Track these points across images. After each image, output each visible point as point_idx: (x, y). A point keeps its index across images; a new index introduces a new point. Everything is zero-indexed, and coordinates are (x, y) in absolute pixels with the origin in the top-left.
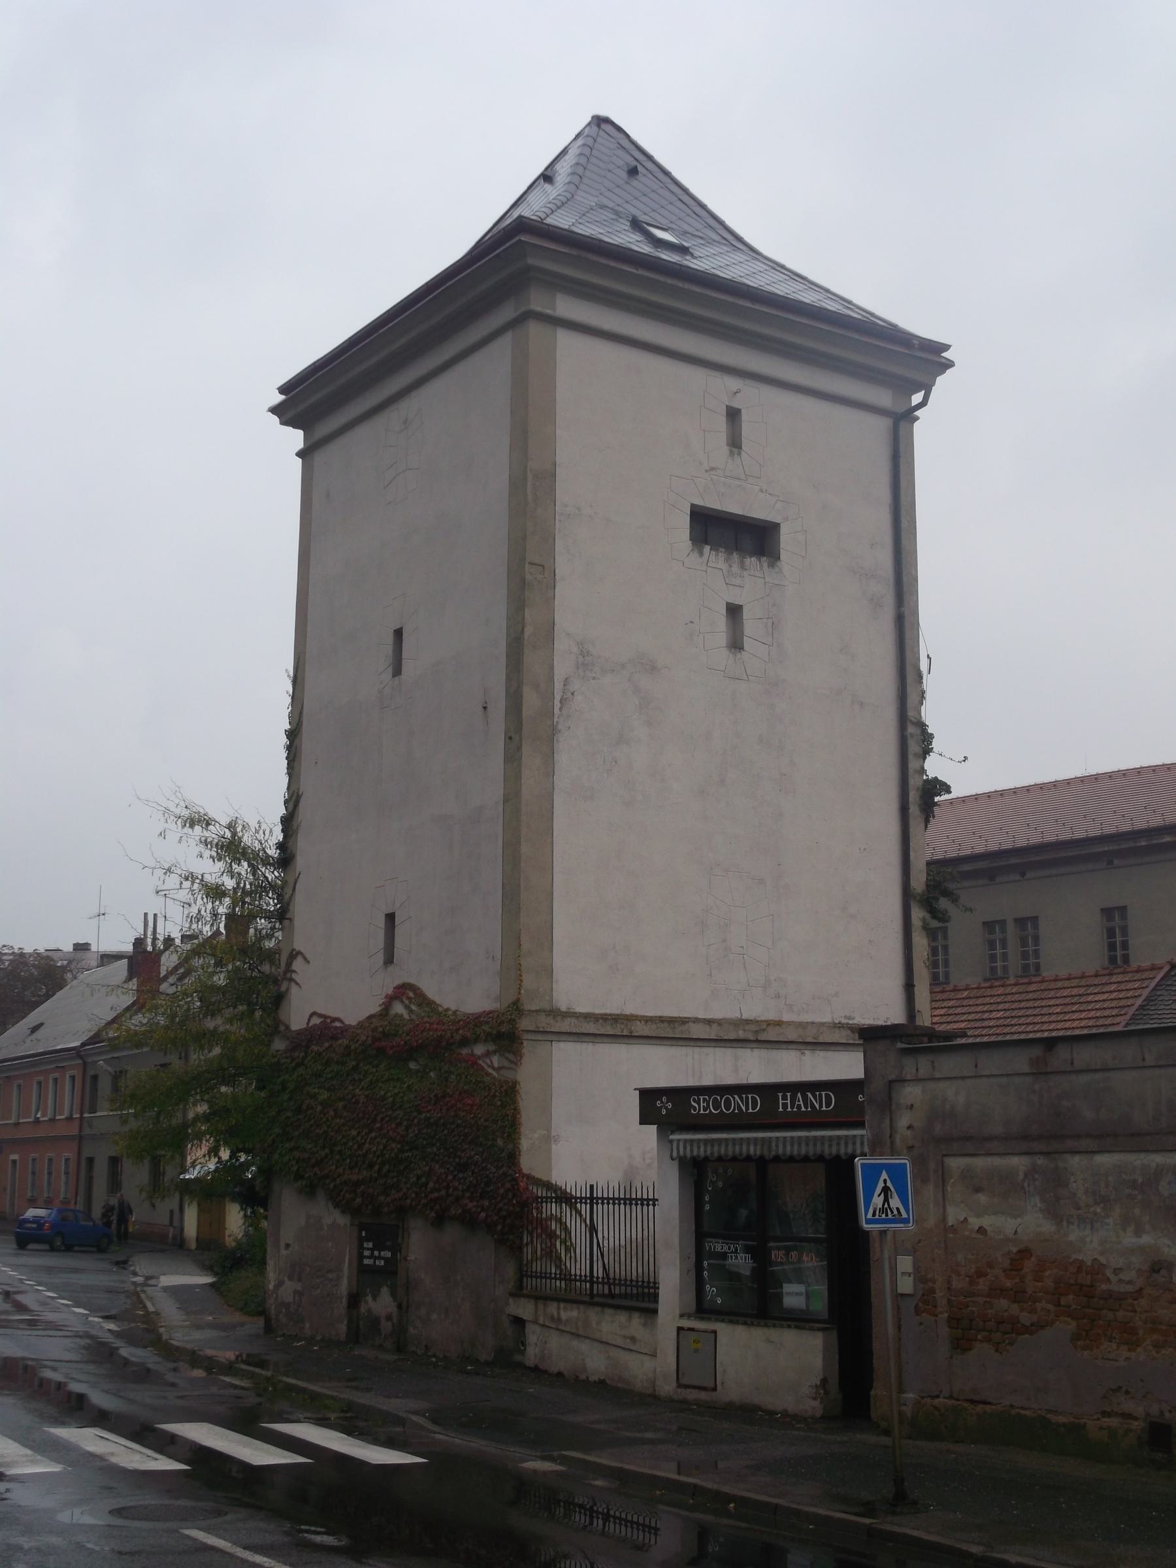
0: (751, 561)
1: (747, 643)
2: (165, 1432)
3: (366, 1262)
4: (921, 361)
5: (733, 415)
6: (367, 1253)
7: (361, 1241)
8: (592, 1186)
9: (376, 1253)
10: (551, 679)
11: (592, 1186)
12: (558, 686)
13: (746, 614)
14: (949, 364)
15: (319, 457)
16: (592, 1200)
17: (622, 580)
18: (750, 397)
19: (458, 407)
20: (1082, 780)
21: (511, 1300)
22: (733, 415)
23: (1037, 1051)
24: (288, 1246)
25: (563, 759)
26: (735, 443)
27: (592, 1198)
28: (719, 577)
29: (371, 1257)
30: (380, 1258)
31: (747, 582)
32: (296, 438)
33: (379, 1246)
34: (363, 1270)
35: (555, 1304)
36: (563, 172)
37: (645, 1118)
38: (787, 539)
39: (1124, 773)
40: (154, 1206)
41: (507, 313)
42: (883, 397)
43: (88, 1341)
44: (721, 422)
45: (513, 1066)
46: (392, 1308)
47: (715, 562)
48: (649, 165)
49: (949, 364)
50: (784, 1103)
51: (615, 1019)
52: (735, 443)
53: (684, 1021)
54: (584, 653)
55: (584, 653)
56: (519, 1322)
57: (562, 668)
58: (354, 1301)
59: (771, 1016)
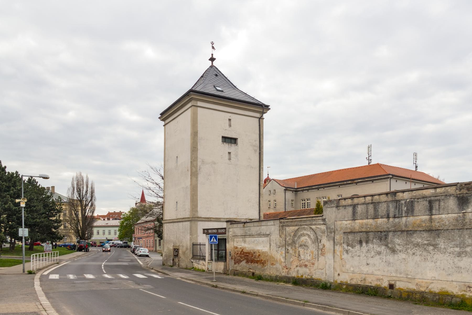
0: (233, 145)
1: (232, 159)
2: (134, 276)
4: (264, 108)
5: (230, 120)
10: (197, 166)
12: (198, 167)
13: (231, 154)
14: (270, 109)
15: (166, 126)
16: (200, 245)
17: (212, 148)
18: (233, 117)
19: (184, 119)
20: (337, 171)
22: (230, 120)
23: (243, 224)
25: (199, 178)
26: (230, 126)
28: (227, 147)
31: (232, 148)
32: (163, 123)
34: (174, 255)
37: (204, 233)
38: (239, 141)
39: (323, 173)
41: (190, 105)
42: (258, 115)
44: (228, 121)
47: (226, 145)
48: (220, 74)
49: (270, 109)
50: (219, 231)
51: (208, 218)
52: (230, 126)
53: (220, 218)
54: (203, 161)
55: (203, 161)
57: (199, 164)
59: (235, 217)
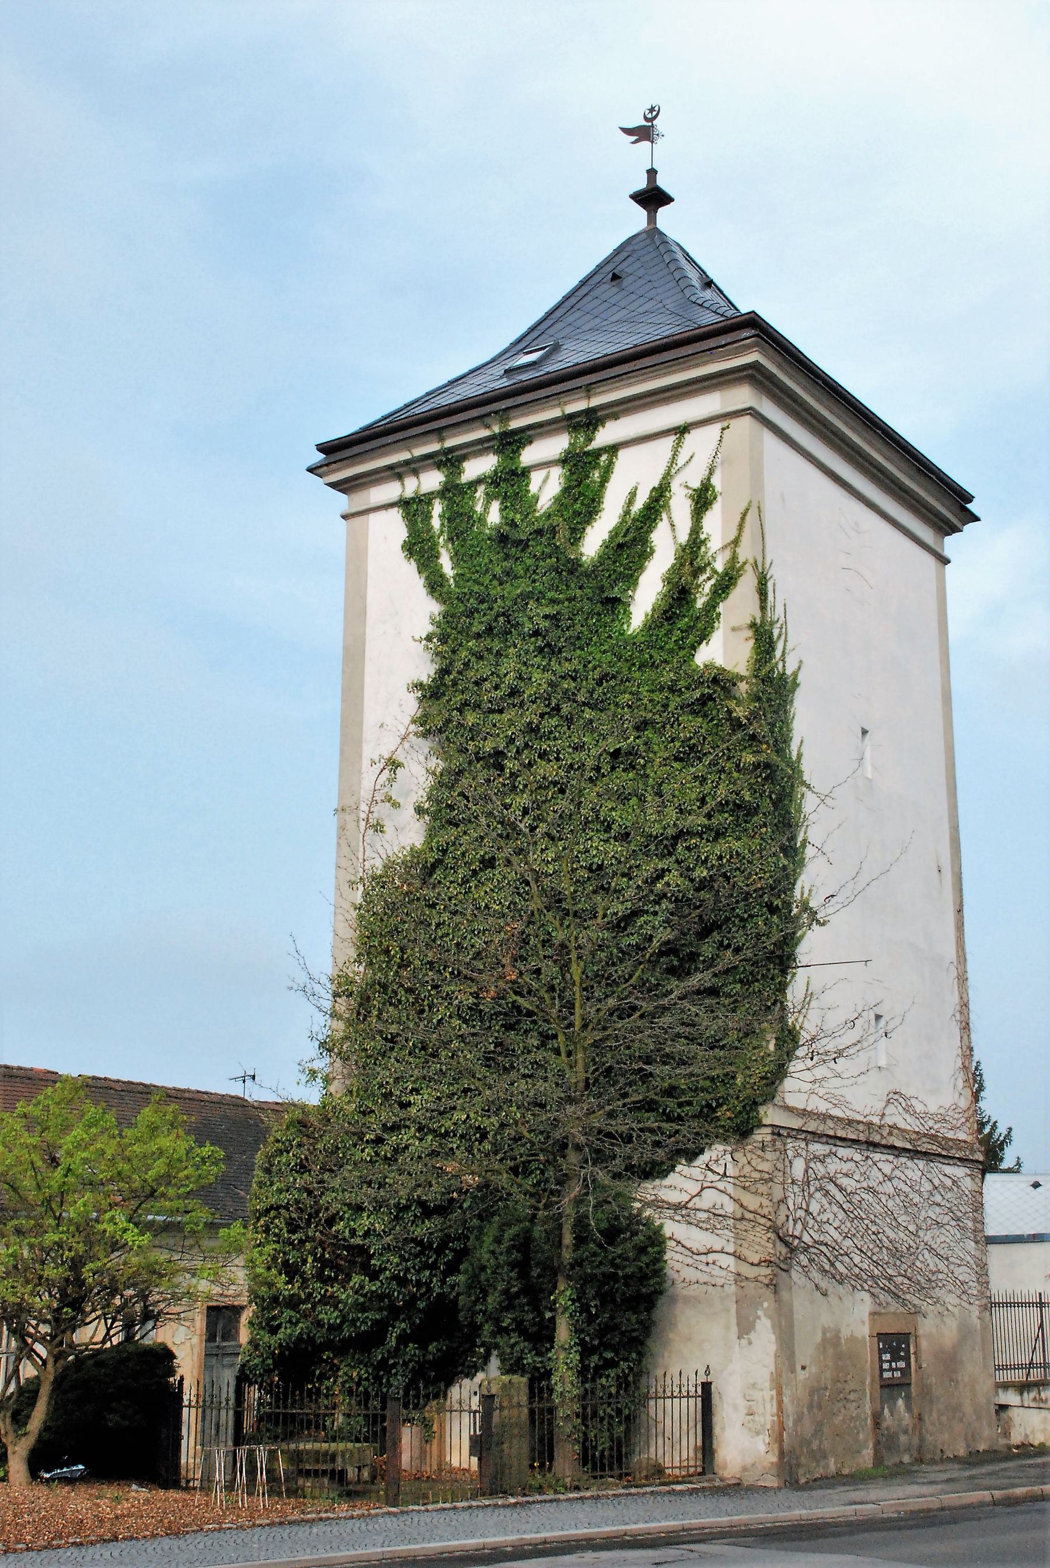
3: (886, 1375)
6: (886, 1366)
7: (881, 1352)
8: (1040, 1294)
9: (893, 1364)
11: (1040, 1294)
21: (1000, 1391)
24: (803, 1368)
27: (1041, 1303)
29: (891, 1369)
30: (897, 1369)
33: (895, 1358)
35: (1036, 1389)
36: (708, 294)
40: (687, 487)
43: (794, 758)
45: (391, 1500)
46: (907, 1419)
56: (1003, 1408)
58: (877, 1419)
